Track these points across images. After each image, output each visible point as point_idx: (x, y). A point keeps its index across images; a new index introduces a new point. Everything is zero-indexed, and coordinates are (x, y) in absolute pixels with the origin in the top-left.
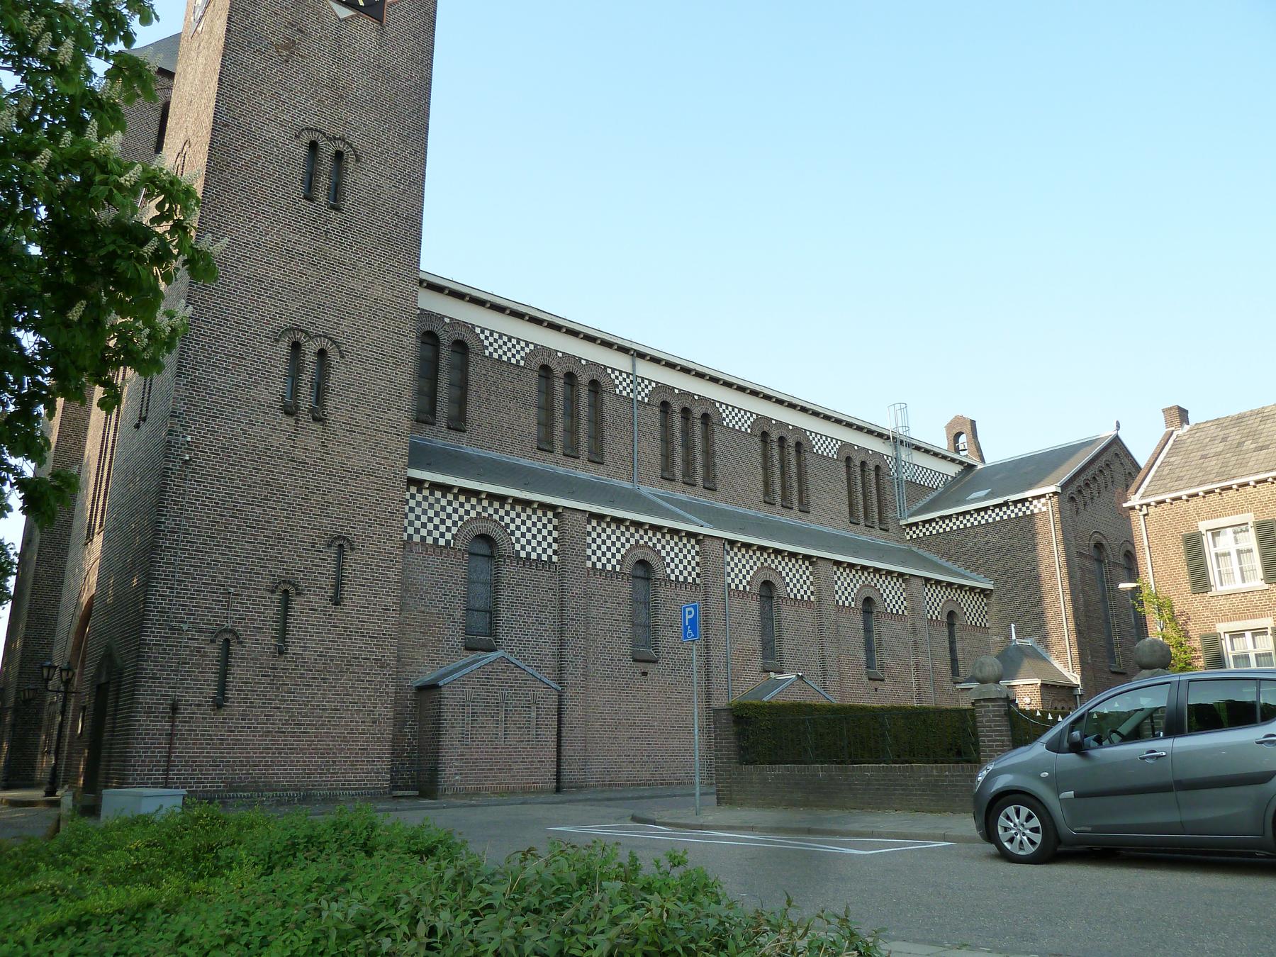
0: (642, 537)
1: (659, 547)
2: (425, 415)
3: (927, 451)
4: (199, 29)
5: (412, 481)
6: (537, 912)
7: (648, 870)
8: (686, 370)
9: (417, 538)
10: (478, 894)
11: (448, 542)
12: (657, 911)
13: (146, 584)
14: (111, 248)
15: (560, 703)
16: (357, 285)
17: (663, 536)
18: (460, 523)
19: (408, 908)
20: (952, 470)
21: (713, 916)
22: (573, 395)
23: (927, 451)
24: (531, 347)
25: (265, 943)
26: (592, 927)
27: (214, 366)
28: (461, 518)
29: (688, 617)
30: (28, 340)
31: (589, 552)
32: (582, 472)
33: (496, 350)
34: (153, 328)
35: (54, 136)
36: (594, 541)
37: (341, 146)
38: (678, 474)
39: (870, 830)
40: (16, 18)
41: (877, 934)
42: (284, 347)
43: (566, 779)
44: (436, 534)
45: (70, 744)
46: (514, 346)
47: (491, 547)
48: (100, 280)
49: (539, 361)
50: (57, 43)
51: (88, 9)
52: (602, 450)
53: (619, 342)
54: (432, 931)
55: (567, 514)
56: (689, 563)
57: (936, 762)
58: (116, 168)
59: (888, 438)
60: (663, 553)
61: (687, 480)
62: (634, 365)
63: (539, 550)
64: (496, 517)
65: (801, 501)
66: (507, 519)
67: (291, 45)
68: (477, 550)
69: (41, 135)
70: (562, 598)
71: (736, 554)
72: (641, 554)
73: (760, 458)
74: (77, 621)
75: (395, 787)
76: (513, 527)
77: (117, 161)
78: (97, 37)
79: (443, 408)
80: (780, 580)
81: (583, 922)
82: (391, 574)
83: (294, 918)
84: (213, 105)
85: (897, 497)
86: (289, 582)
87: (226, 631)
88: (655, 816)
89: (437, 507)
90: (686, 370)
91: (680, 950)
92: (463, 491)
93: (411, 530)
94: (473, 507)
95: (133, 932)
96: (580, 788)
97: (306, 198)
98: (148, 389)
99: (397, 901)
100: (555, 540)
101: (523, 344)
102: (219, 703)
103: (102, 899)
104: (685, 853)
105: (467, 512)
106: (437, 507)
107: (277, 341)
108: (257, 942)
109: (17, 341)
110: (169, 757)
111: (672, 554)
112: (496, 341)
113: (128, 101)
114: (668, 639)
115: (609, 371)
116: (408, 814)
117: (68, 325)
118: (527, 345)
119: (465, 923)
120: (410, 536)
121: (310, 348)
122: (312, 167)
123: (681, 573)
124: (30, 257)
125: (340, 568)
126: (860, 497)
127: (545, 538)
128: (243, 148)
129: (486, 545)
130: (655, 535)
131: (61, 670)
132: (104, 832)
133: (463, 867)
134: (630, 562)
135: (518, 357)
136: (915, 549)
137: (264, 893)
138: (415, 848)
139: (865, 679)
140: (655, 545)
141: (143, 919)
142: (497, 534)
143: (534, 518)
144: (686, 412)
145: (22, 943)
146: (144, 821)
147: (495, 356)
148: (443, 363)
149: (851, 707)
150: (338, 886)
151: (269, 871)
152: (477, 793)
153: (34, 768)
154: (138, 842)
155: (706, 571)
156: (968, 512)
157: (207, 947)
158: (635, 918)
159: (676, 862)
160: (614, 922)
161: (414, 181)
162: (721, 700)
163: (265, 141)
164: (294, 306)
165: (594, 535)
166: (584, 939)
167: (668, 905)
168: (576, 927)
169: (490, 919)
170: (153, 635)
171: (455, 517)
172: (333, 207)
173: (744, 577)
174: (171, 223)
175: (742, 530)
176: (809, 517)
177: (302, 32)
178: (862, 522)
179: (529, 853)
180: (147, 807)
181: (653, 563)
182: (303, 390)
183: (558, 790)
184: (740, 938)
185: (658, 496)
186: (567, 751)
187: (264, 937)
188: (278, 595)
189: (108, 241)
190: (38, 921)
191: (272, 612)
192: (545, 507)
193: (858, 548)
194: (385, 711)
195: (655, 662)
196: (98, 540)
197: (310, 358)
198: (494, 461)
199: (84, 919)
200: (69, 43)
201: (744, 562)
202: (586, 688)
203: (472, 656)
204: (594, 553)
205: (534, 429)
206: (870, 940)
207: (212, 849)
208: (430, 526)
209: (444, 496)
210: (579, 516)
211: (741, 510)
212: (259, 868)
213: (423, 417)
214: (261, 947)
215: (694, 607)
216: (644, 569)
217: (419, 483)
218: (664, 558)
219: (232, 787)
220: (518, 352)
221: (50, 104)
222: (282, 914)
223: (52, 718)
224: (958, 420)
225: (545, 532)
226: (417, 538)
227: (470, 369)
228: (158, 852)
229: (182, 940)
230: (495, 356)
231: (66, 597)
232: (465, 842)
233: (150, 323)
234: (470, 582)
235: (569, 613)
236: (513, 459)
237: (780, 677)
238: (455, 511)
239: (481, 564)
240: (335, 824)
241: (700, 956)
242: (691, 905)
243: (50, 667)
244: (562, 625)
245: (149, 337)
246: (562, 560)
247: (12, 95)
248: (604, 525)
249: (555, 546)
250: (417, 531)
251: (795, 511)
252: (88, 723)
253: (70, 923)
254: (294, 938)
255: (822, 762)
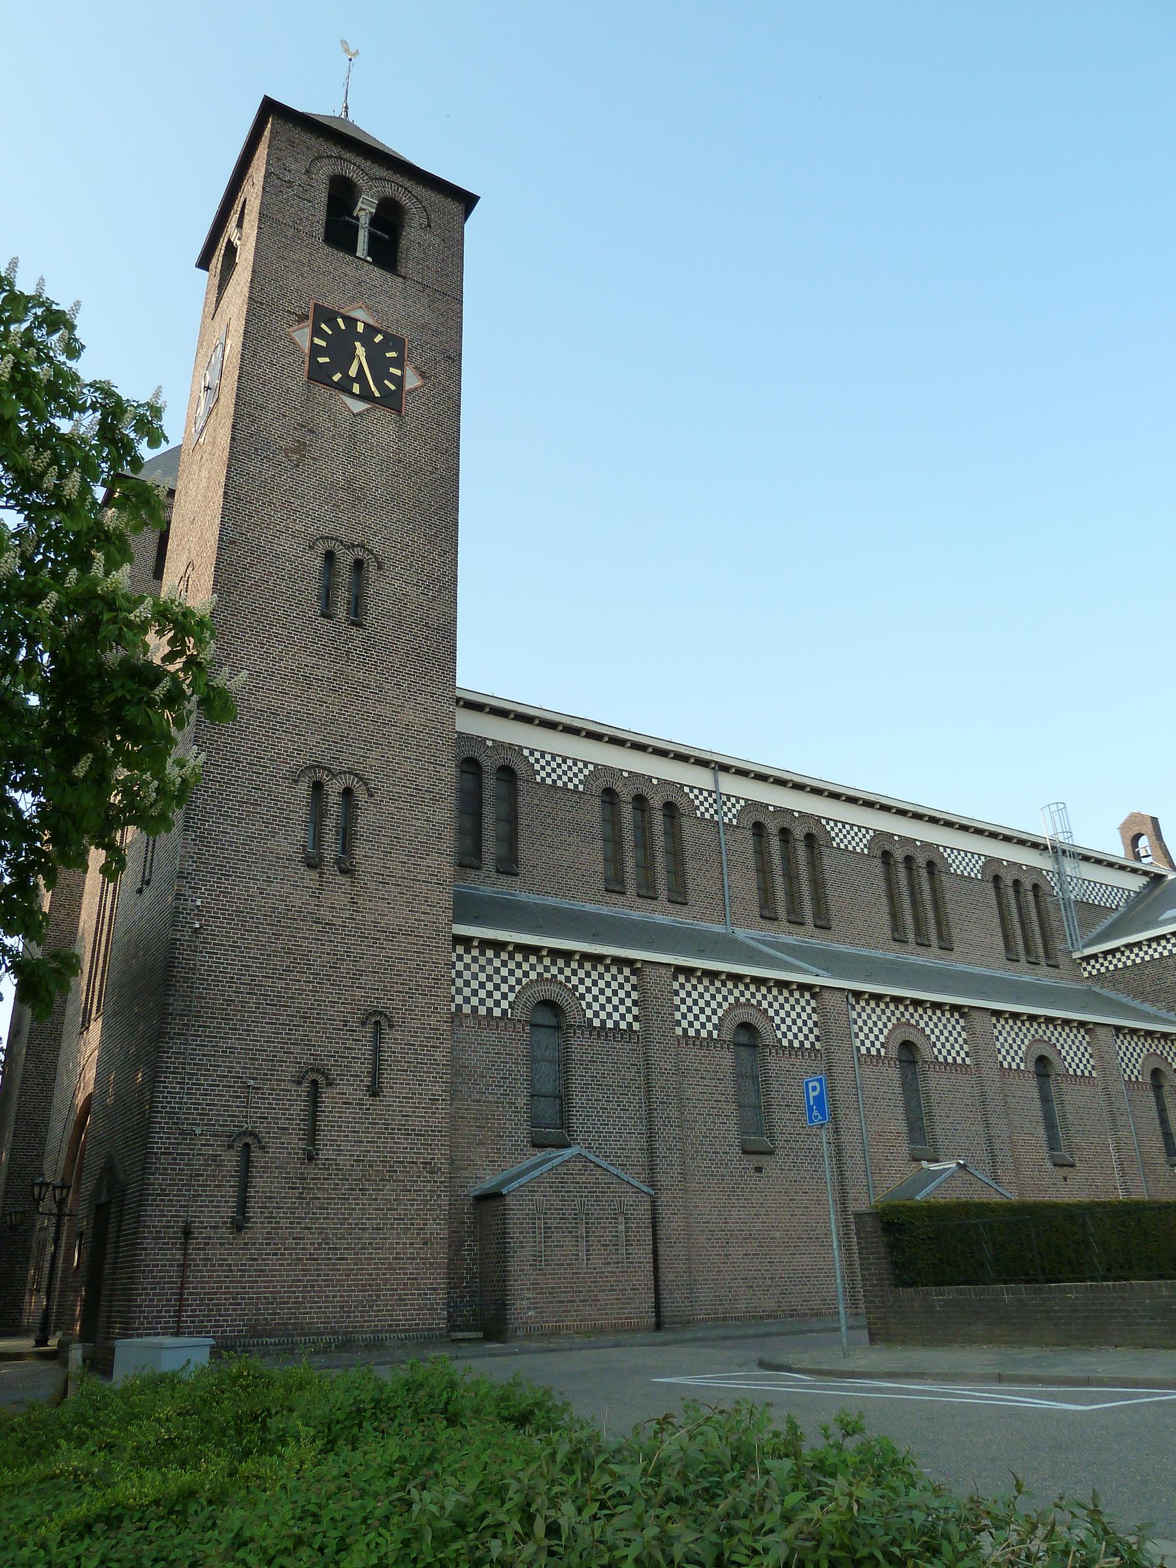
0: (902, 1014)
1: (765, 1004)
2: (469, 858)
3: (1099, 862)
4: (201, 440)
5: (458, 940)
6: (679, 1501)
7: (813, 1445)
8: (780, 782)
9: (467, 1009)
10: (606, 1479)
11: (504, 1012)
12: (844, 1501)
13: (153, 1079)
14: (120, 693)
15: (654, 1210)
16: (387, 712)
17: (770, 991)
18: (518, 988)
19: (518, 1499)
20: (1135, 883)
21: (916, 1507)
22: (646, 823)
23: (1099, 862)
24: (591, 767)
25: (343, 1547)
26: (757, 1523)
27: (226, 816)
28: (519, 981)
29: (812, 1094)
30: (26, 801)
31: (678, 1016)
32: (662, 916)
33: (549, 775)
34: (161, 780)
35: (58, 577)
36: (683, 1001)
37: (360, 553)
38: (782, 912)
39: (1084, 1375)
40: (20, 454)
41: (1142, 1532)
42: (304, 788)
43: (667, 1312)
44: (490, 1003)
45: (64, 1278)
46: (570, 768)
47: (556, 1016)
48: (107, 729)
49: (601, 783)
50: (62, 476)
51: (95, 436)
52: (685, 887)
53: (696, 753)
54: (553, 1530)
55: (648, 970)
56: (805, 1023)
57: (1161, 1277)
58: (125, 604)
59: (1046, 848)
60: (771, 1013)
61: (792, 918)
62: (716, 781)
63: (616, 1016)
64: (561, 978)
65: (940, 936)
66: (575, 980)
67: (301, 448)
68: (540, 1021)
69: (45, 574)
70: (648, 1077)
71: (863, 1009)
72: (743, 1015)
73: (883, 885)
74: (71, 1127)
75: (453, 1328)
76: (582, 989)
77: (124, 596)
78: (103, 465)
79: (490, 848)
80: (923, 1039)
81: (745, 1517)
82: (438, 1055)
83: (378, 1512)
84: (218, 521)
85: (1066, 923)
86: (318, 1071)
87: (245, 1133)
88: (789, 1359)
89: (490, 970)
90: (780, 782)
91: (880, 1556)
92: (520, 948)
93: (459, 999)
94: (533, 967)
95: (173, 1531)
96: (686, 1323)
97: (323, 615)
98: (150, 849)
99: (504, 1489)
100: (635, 1003)
101: (580, 765)
102: (239, 1224)
103: (136, 1487)
104: (861, 1416)
105: (526, 974)
106: (490, 970)
107: (296, 781)
108: (332, 1547)
109: (14, 803)
110: (181, 1294)
111: (937, 1032)
112: (548, 763)
113: (136, 530)
114: (786, 1124)
115: (686, 790)
116: (475, 1363)
117: (73, 782)
118: (586, 766)
119: (595, 1518)
120: (459, 1007)
121: (334, 788)
122: (329, 580)
123: (796, 1036)
124: (31, 710)
125: (377, 1051)
126: (1017, 926)
127: (622, 1001)
128: (252, 565)
129: (551, 1014)
130: (758, 990)
131: (55, 1188)
132: (125, 1394)
133: (581, 1441)
134: (730, 1025)
135: (576, 781)
136: (1097, 989)
137: (335, 1478)
138: (506, 1413)
139: (1049, 1165)
140: (759, 1003)
141: (184, 1512)
142: (563, 999)
143: (608, 977)
144: (785, 833)
145: (44, 1546)
146: (169, 1381)
147: (549, 781)
148: (488, 794)
149: (1037, 1205)
150: (421, 1469)
151: (330, 1446)
152: (556, 1333)
153: (20, 1311)
154: (169, 1410)
155: (828, 1032)
156: (1163, 937)
157: (272, 1552)
158: (814, 1510)
159: (850, 1430)
160: (787, 1519)
161: (444, 586)
162: (861, 1203)
163: (277, 556)
164: (313, 740)
165: (683, 994)
166: (748, 1541)
167: (858, 1493)
168: (738, 1524)
169: (624, 1517)
170: (160, 1143)
171: (512, 981)
172: (354, 624)
173: (877, 1037)
174: (184, 659)
175: (869, 978)
176: (954, 955)
177: (313, 432)
178: (1023, 958)
179: (665, 1422)
180: (169, 1363)
181: (759, 1026)
182: (327, 838)
183: (659, 1326)
184: (956, 1538)
185: (758, 941)
186: (667, 1276)
187: (342, 1539)
188: (305, 1086)
189: (116, 685)
190: (61, 1516)
191: (299, 1107)
192: (620, 962)
193: (895, 973)
194: (438, 1229)
195: (771, 1153)
196: (96, 1028)
197: (333, 798)
198: (555, 908)
199: (114, 1513)
200: (76, 475)
201: (874, 1018)
202: (685, 1190)
203: (541, 1154)
204: (684, 1016)
205: (600, 868)
206: (1132, 1539)
207: (257, 1417)
208: (482, 994)
209: (497, 955)
210: (663, 971)
211: (865, 952)
212: (319, 1443)
213: (467, 860)
214: (338, 1552)
215: (819, 1081)
216: (748, 1035)
217: (466, 941)
218: (772, 1019)
219: (255, 1331)
220: (576, 775)
221: (53, 540)
222: (363, 1507)
223: (42, 1247)
224: (1134, 819)
225: (621, 994)
226: (467, 1009)
227: (520, 799)
228: (193, 1422)
229: (239, 1542)
230: (549, 781)
231: (58, 1097)
232: (567, 1404)
233: (159, 773)
234: (533, 1060)
235: (658, 1094)
236: (577, 905)
237: (934, 1167)
238: (512, 973)
239: (545, 1037)
240: (406, 1383)
241: (910, 1564)
242: (879, 1491)
243: (42, 1185)
244: (650, 1111)
245: (157, 791)
246: (646, 1028)
247: (14, 536)
248: (694, 981)
249: (635, 1011)
250: (467, 1000)
251: (935, 949)
252: (85, 1253)
253: (99, 1518)
254: (380, 1540)
255: (1005, 1282)
